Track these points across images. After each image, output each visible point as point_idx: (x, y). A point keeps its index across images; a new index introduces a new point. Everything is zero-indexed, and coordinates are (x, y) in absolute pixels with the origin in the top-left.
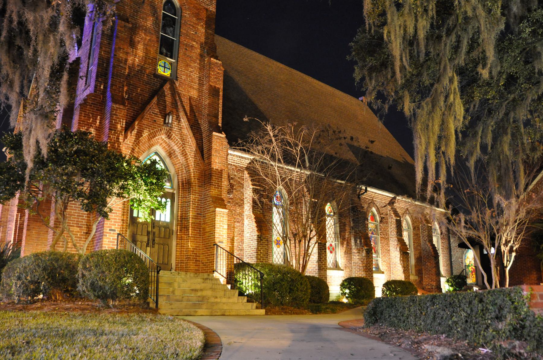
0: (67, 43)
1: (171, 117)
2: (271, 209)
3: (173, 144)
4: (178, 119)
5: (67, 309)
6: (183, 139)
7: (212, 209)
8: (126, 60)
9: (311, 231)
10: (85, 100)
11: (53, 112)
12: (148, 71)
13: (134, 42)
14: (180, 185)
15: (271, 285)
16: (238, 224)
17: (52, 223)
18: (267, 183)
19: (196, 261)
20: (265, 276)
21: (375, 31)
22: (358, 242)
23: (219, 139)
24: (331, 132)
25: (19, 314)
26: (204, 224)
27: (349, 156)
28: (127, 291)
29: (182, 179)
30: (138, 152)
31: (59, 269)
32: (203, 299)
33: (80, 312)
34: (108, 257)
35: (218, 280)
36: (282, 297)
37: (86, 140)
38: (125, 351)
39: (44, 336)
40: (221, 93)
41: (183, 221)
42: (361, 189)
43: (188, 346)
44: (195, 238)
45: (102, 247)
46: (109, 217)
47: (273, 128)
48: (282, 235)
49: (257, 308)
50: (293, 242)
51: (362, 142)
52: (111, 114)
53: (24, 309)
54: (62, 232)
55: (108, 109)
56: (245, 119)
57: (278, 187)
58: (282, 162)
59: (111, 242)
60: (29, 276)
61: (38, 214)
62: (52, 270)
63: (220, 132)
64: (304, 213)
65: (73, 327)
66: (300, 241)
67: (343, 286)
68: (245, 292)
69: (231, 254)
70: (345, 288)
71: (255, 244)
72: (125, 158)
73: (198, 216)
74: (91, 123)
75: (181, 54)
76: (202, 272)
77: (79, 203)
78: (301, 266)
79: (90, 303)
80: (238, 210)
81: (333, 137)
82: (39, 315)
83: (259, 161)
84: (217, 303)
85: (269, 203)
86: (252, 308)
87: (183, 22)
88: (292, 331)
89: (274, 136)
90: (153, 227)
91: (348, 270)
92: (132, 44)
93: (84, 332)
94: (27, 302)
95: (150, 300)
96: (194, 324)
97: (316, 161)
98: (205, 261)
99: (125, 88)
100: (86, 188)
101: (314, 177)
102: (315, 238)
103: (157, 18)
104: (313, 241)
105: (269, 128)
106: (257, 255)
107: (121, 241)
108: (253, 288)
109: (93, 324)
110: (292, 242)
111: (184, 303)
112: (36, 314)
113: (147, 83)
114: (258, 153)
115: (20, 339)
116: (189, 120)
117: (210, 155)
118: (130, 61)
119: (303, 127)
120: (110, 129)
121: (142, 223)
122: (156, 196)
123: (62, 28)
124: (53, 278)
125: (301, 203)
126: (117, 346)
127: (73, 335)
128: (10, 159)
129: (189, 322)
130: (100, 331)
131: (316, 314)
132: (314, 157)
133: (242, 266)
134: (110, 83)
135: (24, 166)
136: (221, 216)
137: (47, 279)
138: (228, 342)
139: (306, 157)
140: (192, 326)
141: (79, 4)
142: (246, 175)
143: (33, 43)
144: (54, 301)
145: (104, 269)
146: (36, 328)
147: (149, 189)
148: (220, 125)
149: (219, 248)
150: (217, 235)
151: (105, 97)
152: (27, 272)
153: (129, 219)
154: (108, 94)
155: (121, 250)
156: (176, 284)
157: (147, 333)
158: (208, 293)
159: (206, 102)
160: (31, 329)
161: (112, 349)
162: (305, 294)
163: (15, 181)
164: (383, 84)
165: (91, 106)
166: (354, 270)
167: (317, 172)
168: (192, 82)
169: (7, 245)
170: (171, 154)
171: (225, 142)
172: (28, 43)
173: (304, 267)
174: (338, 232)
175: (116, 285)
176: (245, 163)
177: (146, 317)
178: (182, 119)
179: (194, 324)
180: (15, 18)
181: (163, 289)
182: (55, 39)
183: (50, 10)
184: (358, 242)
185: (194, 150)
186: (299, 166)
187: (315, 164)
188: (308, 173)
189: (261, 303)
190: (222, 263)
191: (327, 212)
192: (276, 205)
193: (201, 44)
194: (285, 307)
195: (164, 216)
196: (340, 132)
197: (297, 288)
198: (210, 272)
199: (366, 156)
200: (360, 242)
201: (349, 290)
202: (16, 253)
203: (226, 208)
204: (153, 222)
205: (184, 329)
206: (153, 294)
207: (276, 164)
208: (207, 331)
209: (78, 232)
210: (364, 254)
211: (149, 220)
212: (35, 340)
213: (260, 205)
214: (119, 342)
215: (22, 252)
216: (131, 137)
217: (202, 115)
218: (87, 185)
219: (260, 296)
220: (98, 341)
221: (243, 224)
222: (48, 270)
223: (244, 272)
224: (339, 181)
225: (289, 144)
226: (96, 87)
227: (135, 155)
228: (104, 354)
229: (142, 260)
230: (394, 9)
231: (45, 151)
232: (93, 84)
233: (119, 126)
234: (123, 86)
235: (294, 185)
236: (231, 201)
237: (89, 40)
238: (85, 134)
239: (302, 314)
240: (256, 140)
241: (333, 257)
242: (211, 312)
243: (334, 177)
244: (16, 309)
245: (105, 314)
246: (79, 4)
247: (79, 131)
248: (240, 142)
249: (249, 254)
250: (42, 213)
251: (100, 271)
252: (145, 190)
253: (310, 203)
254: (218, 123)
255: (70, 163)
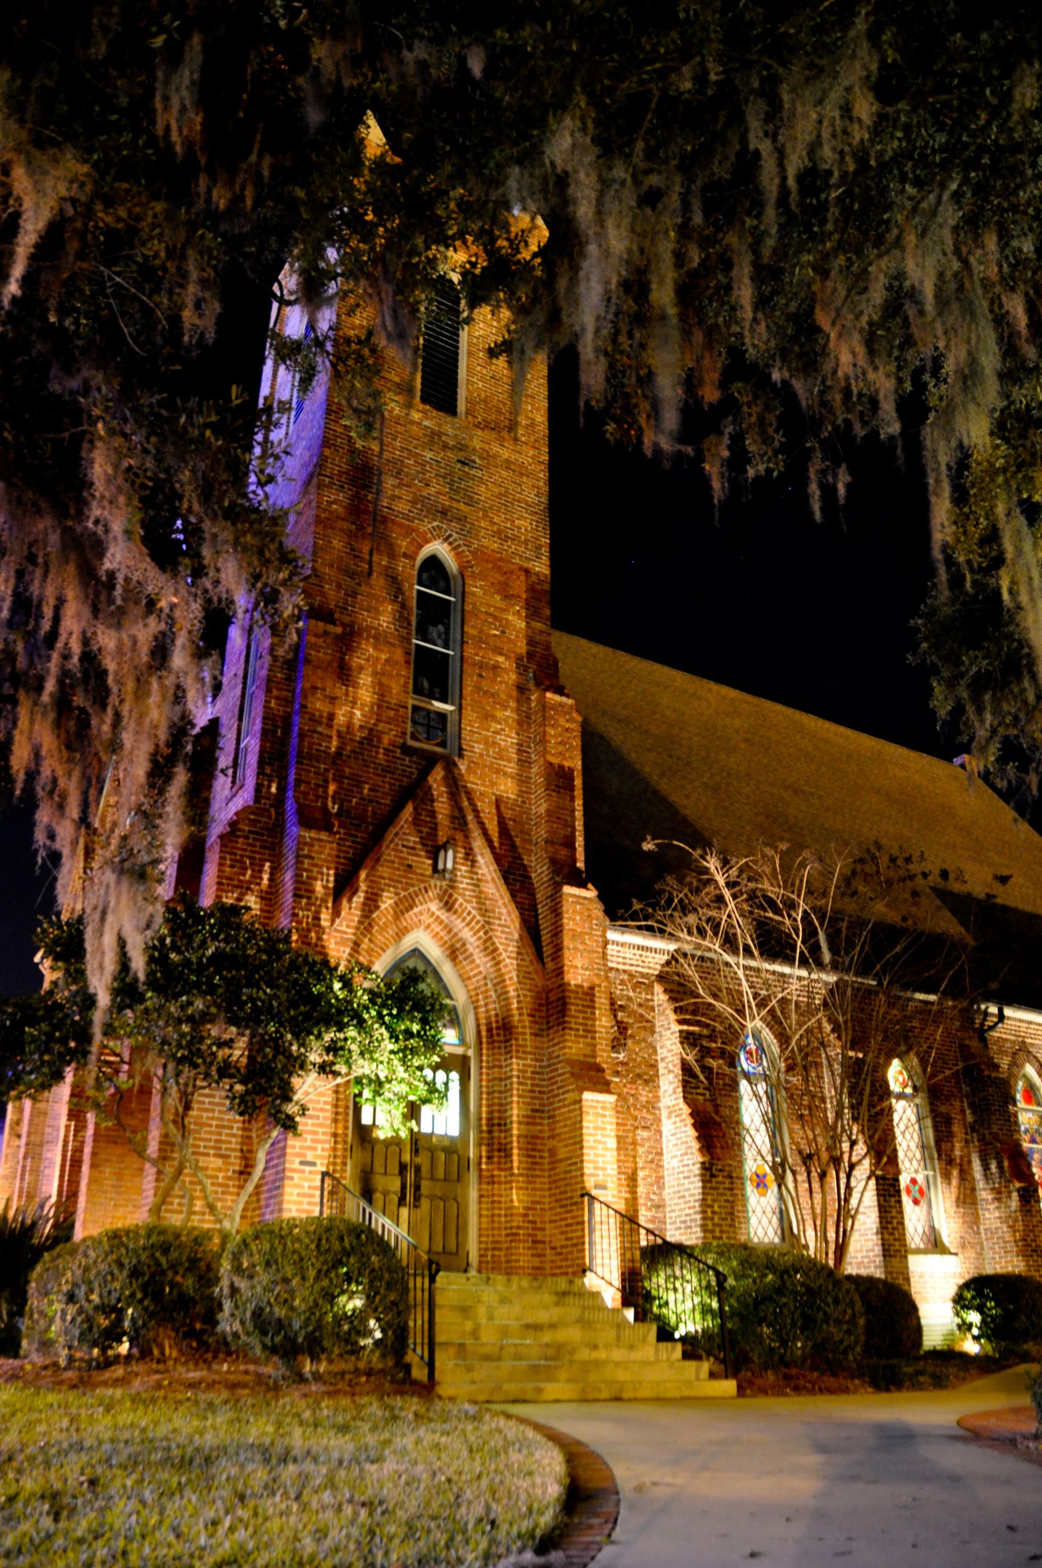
0: (191, 695)
1: (450, 853)
2: (734, 1086)
3: (459, 924)
4: (470, 856)
5: (192, 1385)
6: (484, 911)
7: (571, 1096)
8: (331, 717)
9: (853, 1143)
10: (233, 824)
11: (156, 862)
12: (386, 740)
13: (350, 669)
14: (484, 1034)
15: (747, 1305)
16: (645, 1134)
17: (153, 1148)
18: (719, 1017)
19: (534, 1242)
20: (731, 1282)
21: (974, 582)
22: (993, 1167)
23: (580, 901)
24: (884, 861)
25: (71, 1396)
26: (552, 1137)
27: (947, 924)
28: (349, 1333)
29: (488, 1018)
30: (370, 952)
31: (170, 1274)
32: (557, 1352)
33: (225, 1394)
34: (298, 1240)
35: (596, 1295)
36: (784, 1343)
37: (238, 927)
38: (348, 1510)
39: (132, 1463)
40: (578, 782)
41: (493, 1130)
42: (986, 1014)
43: (523, 1496)
44: (530, 1178)
45: (280, 1210)
46: (300, 1128)
47: (725, 863)
48: (769, 1158)
49: (712, 1375)
50: (802, 1177)
51: (977, 882)
52: (298, 856)
53: (82, 1384)
54: (179, 1172)
55: (289, 845)
56: (648, 846)
57: (749, 1025)
58: (756, 953)
59: (304, 1195)
60: (97, 1291)
61: (120, 1124)
62: (153, 1276)
63: (582, 885)
64: (829, 1092)
65: (209, 1439)
66: (823, 1176)
67: (960, 1301)
68: (677, 1328)
69: (629, 1220)
70: (966, 1307)
71: (695, 1187)
72: (336, 969)
73: (535, 1115)
74: (250, 882)
75: (468, 690)
76: (553, 1275)
77: (224, 1094)
78: (832, 1247)
79: (251, 1367)
80: (644, 1094)
81: (892, 874)
82: (121, 1401)
83: (693, 957)
84: (597, 1364)
85: (728, 1070)
86: (697, 1377)
87: (468, 608)
88: (822, 1448)
89: (727, 884)
90: (416, 1151)
91: (971, 1253)
92: (344, 674)
93: (237, 1454)
94: (89, 1362)
95: (411, 1358)
96: (537, 1427)
97: (850, 945)
98: (559, 1241)
99: (332, 788)
100: (238, 1053)
101: (849, 991)
102: (866, 1162)
103: (403, 606)
104: (862, 1171)
105: (712, 864)
106: (704, 1219)
107: (331, 1193)
108: (698, 1316)
109: (260, 1429)
110: (799, 1178)
111: (507, 1365)
112: (112, 1397)
113: (386, 770)
114: (690, 933)
115: (72, 1472)
116: (498, 859)
117: (558, 949)
118: (341, 719)
119: (806, 854)
120: (295, 895)
121: (385, 1140)
122: (420, 1068)
123: (179, 659)
124: (157, 1295)
125: (818, 1065)
126: (327, 1496)
127: (208, 1460)
128: (55, 983)
129: (522, 1420)
130: (279, 1449)
131: (888, 1390)
132: (843, 935)
133: (663, 1253)
134: (292, 777)
135: (89, 1001)
136: (598, 1115)
137: (141, 1301)
138: (634, 1483)
139: (822, 936)
140: (531, 1434)
141: (220, 601)
142: (660, 996)
143: (113, 700)
144: (158, 1362)
145: (289, 1271)
146: (112, 1441)
147: (403, 1050)
148: (580, 865)
149: (597, 1205)
150: (588, 1169)
151: (281, 814)
152: (90, 1282)
153: (350, 1132)
154: (290, 806)
155: (330, 1219)
156: (480, 1309)
157: (408, 1457)
158: (572, 1334)
159: (540, 807)
160: (100, 1443)
161: (314, 1505)
162: (849, 1332)
163: (64, 1041)
164: (1016, 718)
165: (247, 838)
166: (988, 1254)
167: (856, 974)
168: (501, 758)
169: (42, 1207)
170: (455, 952)
171: (597, 910)
172: (102, 702)
173: (841, 1249)
174: (932, 1143)
175: (321, 1318)
176: (654, 963)
177: (402, 1409)
178: (479, 858)
179: (537, 1427)
180: (76, 648)
181: (449, 1326)
182: (162, 686)
183: (152, 621)
184: (993, 1167)
185: (516, 936)
186: (804, 963)
187: (847, 953)
188: (832, 978)
189: (723, 1361)
190: (605, 1247)
191: (895, 1087)
192: (747, 1076)
193: (519, 659)
194: (794, 1371)
195: (443, 1120)
196: (908, 860)
197: (825, 1313)
198: (574, 1273)
199: (985, 915)
200: (1000, 1167)
201: (982, 1313)
202: (64, 1229)
203: (608, 1091)
204: (417, 1141)
205: (508, 1444)
206: (419, 1341)
207: (738, 963)
208: (575, 1449)
209: (219, 1170)
210: (1014, 1202)
211: (404, 1134)
212: (109, 1475)
213: (702, 1077)
214: (331, 1483)
215: (78, 1226)
216: (352, 910)
217: (530, 842)
218: (242, 1043)
219: (718, 1340)
220: (274, 1480)
221: (660, 1132)
222: (143, 1274)
223: (669, 1272)
224: (921, 996)
225: (772, 903)
226: (258, 788)
227: (361, 959)
228: (293, 1519)
229: (388, 1244)
230: (1021, 521)
231: (139, 964)
232: (250, 782)
233: (318, 887)
234: (326, 781)
235: (794, 1016)
236: (621, 1068)
237: (241, 673)
238: (235, 910)
239: (846, 1390)
240: (681, 901)
241: (923, 1216)
242: (584, 1390)
243: (905, 987)
244: (61, 1383)
245: (292, 1399)
246: (220, 601)
247: (220, 907)
248: (637, 906)
249: (682, 1224)
250: (127, 1121)
251: (279, 1277)
252: (392, 1052)
253: (842, 1064)
254: (575, 861)
255: (199, 988)
